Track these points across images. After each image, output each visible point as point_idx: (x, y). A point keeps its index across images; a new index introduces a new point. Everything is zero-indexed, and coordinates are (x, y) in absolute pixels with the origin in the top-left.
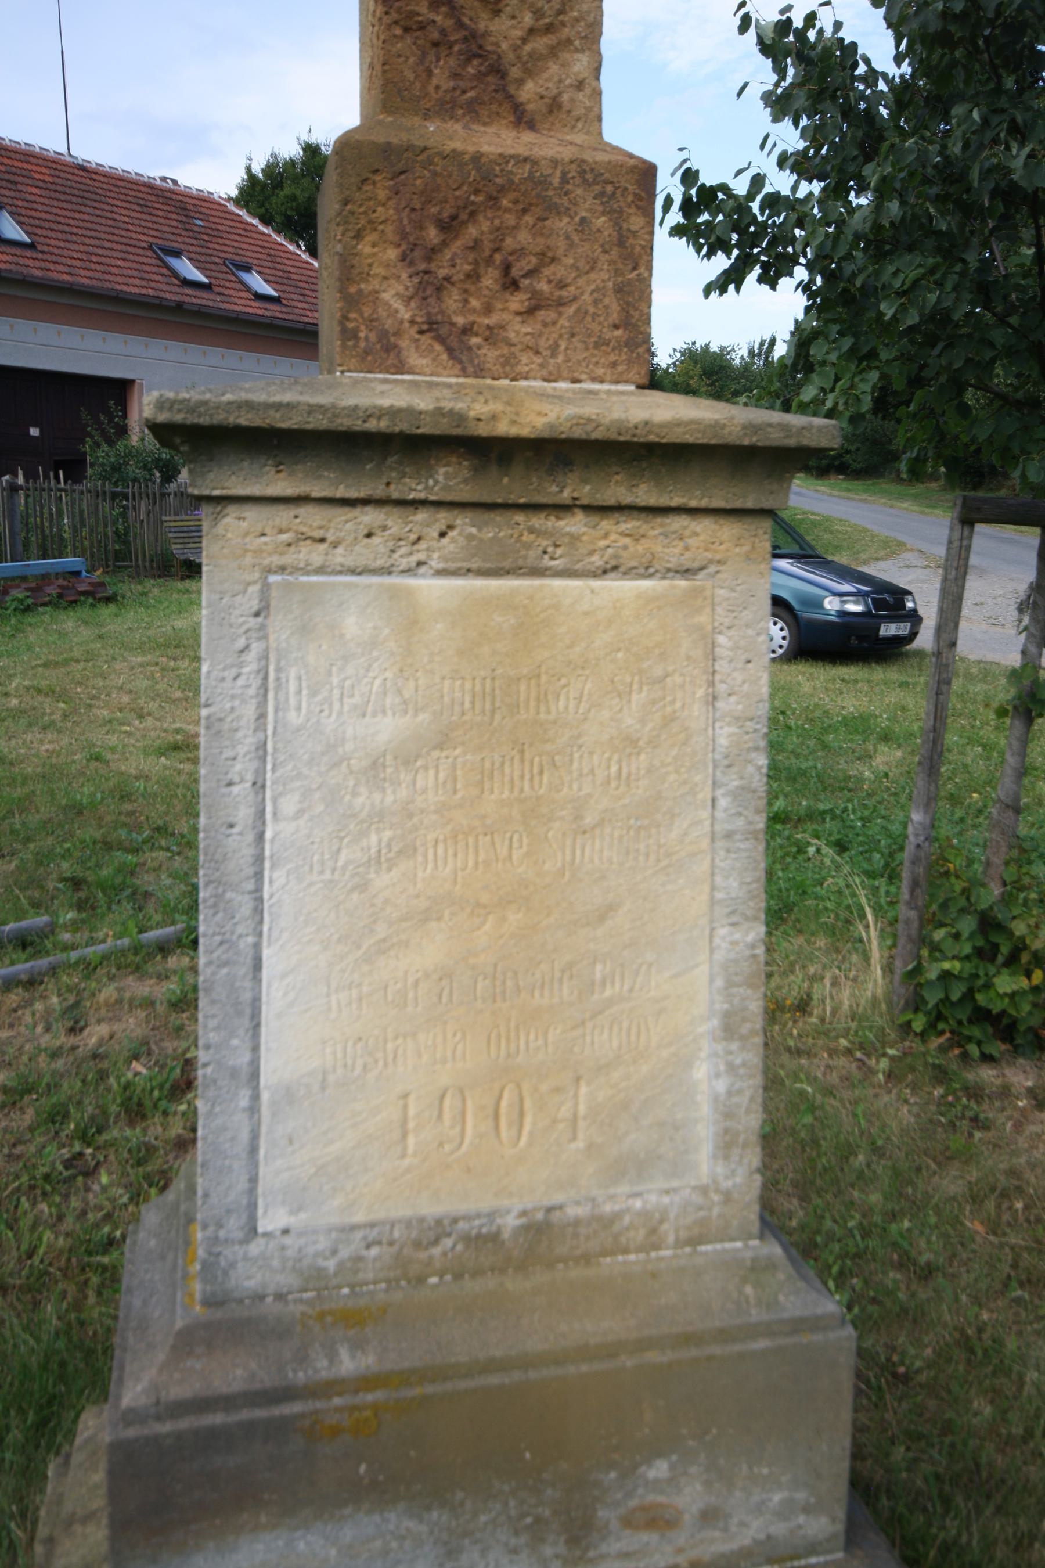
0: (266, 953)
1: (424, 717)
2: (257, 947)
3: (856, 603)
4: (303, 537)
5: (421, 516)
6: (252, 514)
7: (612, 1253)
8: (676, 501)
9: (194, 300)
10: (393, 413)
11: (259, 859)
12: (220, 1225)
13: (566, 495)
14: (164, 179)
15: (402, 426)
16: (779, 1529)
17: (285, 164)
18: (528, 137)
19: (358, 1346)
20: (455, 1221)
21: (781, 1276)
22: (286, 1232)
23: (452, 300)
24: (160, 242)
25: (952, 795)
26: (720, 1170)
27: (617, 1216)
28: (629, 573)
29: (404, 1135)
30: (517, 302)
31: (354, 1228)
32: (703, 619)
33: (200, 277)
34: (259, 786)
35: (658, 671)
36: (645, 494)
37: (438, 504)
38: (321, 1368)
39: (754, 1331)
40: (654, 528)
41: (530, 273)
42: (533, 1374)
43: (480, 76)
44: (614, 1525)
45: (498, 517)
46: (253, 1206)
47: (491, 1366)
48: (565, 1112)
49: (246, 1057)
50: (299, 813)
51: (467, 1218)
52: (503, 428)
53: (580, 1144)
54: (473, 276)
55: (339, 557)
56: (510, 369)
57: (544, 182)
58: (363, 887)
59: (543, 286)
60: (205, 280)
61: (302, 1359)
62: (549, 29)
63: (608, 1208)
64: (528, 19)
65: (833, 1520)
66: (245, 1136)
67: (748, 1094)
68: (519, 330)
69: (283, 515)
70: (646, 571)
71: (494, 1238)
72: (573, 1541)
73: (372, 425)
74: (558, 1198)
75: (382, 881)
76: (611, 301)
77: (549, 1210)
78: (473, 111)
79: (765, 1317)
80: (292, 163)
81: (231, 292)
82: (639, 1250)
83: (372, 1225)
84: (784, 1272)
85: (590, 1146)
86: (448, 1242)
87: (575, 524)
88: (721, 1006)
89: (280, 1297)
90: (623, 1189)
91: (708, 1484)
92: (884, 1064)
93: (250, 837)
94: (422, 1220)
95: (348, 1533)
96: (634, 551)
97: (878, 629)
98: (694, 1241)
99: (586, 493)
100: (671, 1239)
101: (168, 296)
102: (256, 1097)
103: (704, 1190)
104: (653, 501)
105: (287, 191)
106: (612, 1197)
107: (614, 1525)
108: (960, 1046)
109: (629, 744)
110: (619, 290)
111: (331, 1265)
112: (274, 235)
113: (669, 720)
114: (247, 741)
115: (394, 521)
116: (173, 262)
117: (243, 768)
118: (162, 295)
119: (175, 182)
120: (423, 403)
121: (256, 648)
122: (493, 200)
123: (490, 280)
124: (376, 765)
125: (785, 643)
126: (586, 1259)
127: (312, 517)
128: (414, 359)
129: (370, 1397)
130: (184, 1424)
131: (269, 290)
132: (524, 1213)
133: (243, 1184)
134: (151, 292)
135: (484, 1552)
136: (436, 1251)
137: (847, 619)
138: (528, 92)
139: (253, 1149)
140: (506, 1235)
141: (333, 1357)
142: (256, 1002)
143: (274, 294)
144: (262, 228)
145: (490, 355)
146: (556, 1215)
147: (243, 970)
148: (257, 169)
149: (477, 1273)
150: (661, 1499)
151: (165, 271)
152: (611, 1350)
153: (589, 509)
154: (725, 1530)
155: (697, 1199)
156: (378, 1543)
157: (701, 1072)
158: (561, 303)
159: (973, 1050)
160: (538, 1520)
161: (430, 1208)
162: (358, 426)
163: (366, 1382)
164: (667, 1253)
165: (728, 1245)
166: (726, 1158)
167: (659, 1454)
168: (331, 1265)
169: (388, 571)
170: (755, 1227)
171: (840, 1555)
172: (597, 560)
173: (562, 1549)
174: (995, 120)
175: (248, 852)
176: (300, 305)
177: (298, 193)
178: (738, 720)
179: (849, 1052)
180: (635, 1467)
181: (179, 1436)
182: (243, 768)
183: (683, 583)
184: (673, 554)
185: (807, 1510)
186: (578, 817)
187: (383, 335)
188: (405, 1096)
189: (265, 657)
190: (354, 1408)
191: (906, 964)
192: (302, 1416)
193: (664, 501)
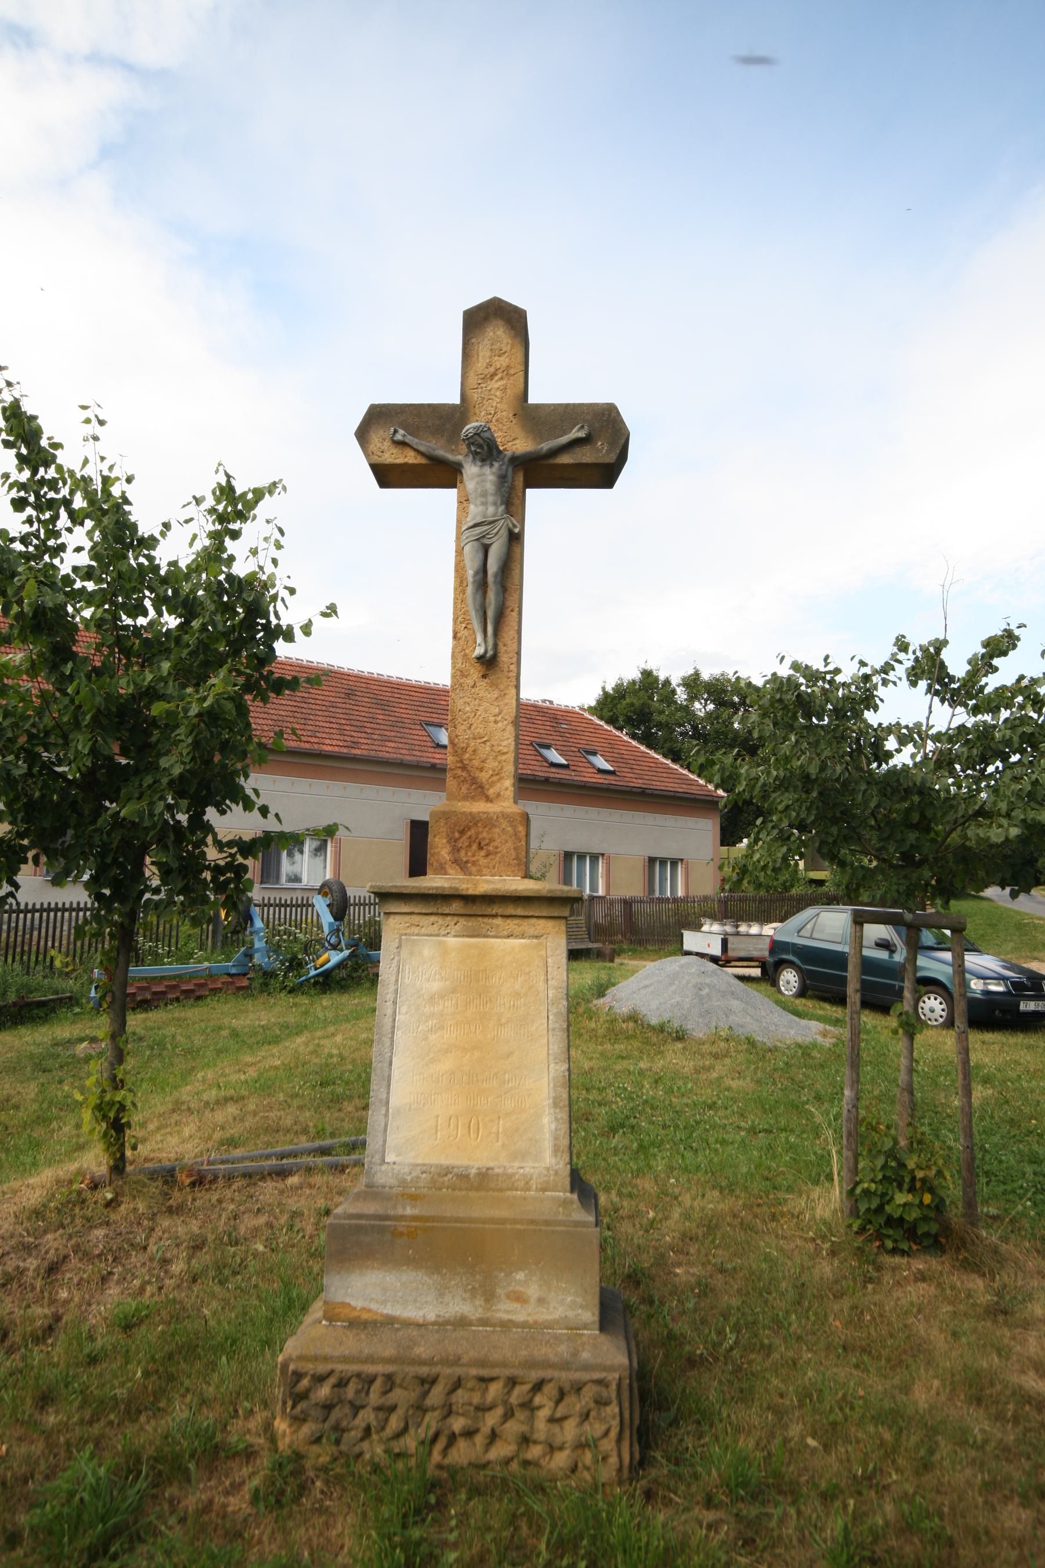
0: (394, 1059)
1: (448, 983)
2: (391, 1057)
3: (999, 984)
4: (412, 925)
5: (449, 918)
6: (398, 918)
7: (511, 1190)
8: (531, 914)
9: (557, 776)
10: (437, 888)
11: (393, 1027)
12: (373, 1157)
13: (494, 912)
14: (544, 701)
15: (440, 892)
16: (571, 1314)
17: (629, 683)
18: (489, 805)
19: (413, 1207)
20: (453, 1168)
21: (575, 1206)
22: (394, 1163)
23: (462, 853)
24: (538, 740)
25: (1012, 1119)
26: (553, 1161)
27: (513, 1175)
28: (517, 937)
29: (437, 1132)
30: (483, 853)
31: (418, 1165)
32: (543, 953)
33: (562, 761)
34: (395, 1003)
35: (527, 970)
36: (520, 912)
37: (454, 915)
38: (400, 1211)
39: (559, 1223)
40: (525, 923)
41: (487, 845)
42: (473, 1225)
43: (476, 789)
44: (503, 1297)
45: (473, 919)
46: (384, 1151)
47: (458, 1220)
48: (494, 1129)
49: (385, 1096)
50: (407, 1013)
51: (458, 1167)
52: (470, 892)
53: (500, 1144)
54: (470, 846)
55: (423, 930)
56: (480, 873)
57: (491, 819)
58: (426, 1039)
59: (491, 848)
60: (565, 762)
61: (394, 1207)
62: (497, 774)
63: (510, 1171)
64: (491, 772)
65: (593, 1315)
66: (383, 1125)
67: (563, 1131)
68: (483, 862)
69: (407, 918)
70: (523, 936)
71: (467, 1176)
72: (487, 1300)
73: (431, 892)
74: (491, 1164)
75: (432, 1037)
76: (513, 852)
77: (488, 1169)
78: (473, 798)
79: (564, 1218)
80: (634, 682)
81: (582, 769)
82: (522, 1190)
83: (424, 1165)
84: (577, 1204)
85: (503, 1145)
86: (450, 1176)
87: (498, 921)
88: (552, 1094)
89: (391, 1187)
90: (516, 1164)
91: (540, 1286)
92: (827, 1245)
93: (391, 1019)
94: (441, 1166)
95: (404, 1278)
96: (518, 930)
97: (1019, 1006)
98: (544, 1190)
99: (500, 911)
100: (534, 1187)
101: (540, 774)
102: (387, 1111)
103: (548, 1169)
104: (522, 914)
105: (628, 700)
106: (512, 1167)
107: (503, 1297)
108: (880, 1240)
109: (517, 995)
110: (515, 848)
111: (409, 1178)
112: (614, 731)
113: (531, 988)
114: (392, 988)
115: (440, 920)
116: (545, 752)
117: (390, 997)
118: (536, 773)
119: (551, 702)
120: (446, 885)
121: (396, 959)
122: (476, 824)
123: (475, 847)
124: (432, 998)
125: (944, 1014)
126: (501, 1190)
127: (415, 919)
128: (450, 871)
129: (414, 1224)
130: (353, 1222)
131: (608, 767)
132: (478, 1168)
133: (381, 1142)
134: (529, 772)
135: (453, 1297)
136: (446, 1179)
137: (988, 997)
138: (491, 792)
139: (385, 1130)
140: (471, 1176)
141: (404, 1209)
142: (389, 1076)
143: (611, 769)
144: (606, 727)
145: (474, 869)
146: (490, 1172)
147: (386, 1065)
148: (609, 689)
149: (460, 1189)
150: (522, 1289)
151: (539, 758)
152: (503, 1221)
153: (503, 916)
154: (548, 1309)
155: (545, 1172)
156: (414, 1285)
157: (546, 1120)
158: (496, 853)
159: (889, 1244)
160: (473, 1288)
161: (445, 1161)
162: (426, 892)
163: (415, 1218)
164: (533, 1193)
165: (557, 1193)
166: (556, 1156)
167: (522, 1270)
168: (409, 1178)
169: (438, 935)
170: (568, 1187)
171: (597, 1332)
172: (505, 933)
173: (482, 1303)
174: (802, 740)
175: (390, 1024)
176: (629, 775)
177: (635, 701)
178: (556, 988)
179: (813, 1240)
180: (511, 1273)
181: (350, 1225)
182: (390, 997)
183: (535, 941)
184: (532, 931)
185: (582, 1307)
186: (499, 1020)
187: (441, 864)
188: (437, 1117)
189: (399, 961)
190: (408, 1227)
191: (848, 1185)
192: (390, 1226)
193: (526, 914)
